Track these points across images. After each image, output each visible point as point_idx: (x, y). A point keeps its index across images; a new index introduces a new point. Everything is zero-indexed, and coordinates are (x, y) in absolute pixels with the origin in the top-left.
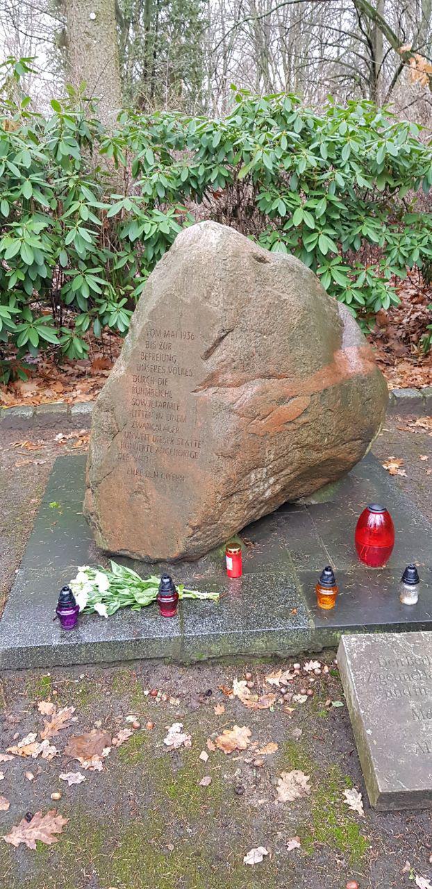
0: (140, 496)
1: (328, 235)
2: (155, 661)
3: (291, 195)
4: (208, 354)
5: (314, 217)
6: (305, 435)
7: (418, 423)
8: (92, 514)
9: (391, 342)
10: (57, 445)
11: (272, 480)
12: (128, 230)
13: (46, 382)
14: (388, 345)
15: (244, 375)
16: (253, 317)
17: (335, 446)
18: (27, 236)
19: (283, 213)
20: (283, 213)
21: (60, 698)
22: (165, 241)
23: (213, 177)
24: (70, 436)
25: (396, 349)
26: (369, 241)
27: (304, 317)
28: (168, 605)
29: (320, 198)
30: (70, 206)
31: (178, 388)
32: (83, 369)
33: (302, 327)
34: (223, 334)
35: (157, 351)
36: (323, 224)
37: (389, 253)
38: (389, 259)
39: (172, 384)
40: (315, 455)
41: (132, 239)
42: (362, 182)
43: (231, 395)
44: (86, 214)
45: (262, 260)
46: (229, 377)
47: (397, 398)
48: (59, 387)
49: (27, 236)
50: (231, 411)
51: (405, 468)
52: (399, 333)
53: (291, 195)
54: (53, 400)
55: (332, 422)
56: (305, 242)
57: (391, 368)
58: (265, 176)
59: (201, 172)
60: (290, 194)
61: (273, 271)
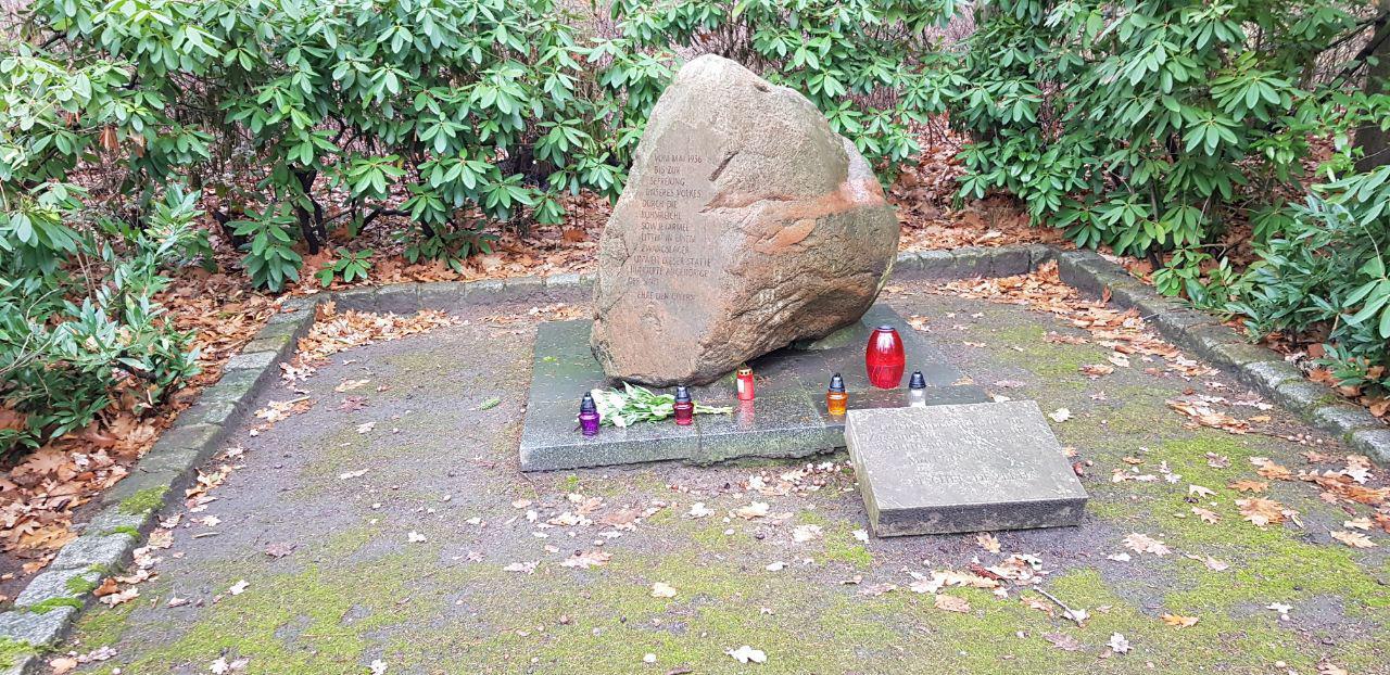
0: (650, 319)
1: (834, 77)
2: (673, 463)
3: (792, 34)
4: (715, 176)
5: (818, 57)
6: (812, 258)
7: (949, 286)
8: (601, 344)
9: (920, 204)
10: (533, 317)
11: (780, 304)
12: (610, 76)
13: (511, 255)
14: (916, 207)
15: (750, 195)
16: (756, 142)
17: (844, 275)
18: (503, 84)
19: (782, 52)
20: (782, 52)
21: (586, 490)
22: (652, 88)
23: (704, 16)
24: (547, 309)
25: (926, 212)
26: (882, 83)
27: (805, 142)
28: (682, 415)
29: (824, 36)
30: (546, 52)
31: (687, 210)
32: (552, 242)
33: (806, 152)
35: (666, 175)
36: (828, 64)
37: (906, 96)
38: (906, 102)
39: (681, 205)
40: (823, 283)
41: (615, 86)
42: (869, 18)
43: (737, 214)
44: (564, 60)
45: (762, 89)
46: (736, 197)
47: (923, 260)
48: (527, 261)
49: (503, 84)
51: (929, 324)
52: (929, 195)
53: (792, 34)
54: (520, 273)
55: (839, 250)
56: (810, 84)
57: (918, 231)
58: (761, 14)
59: (691, 10)
60: (790, 32)
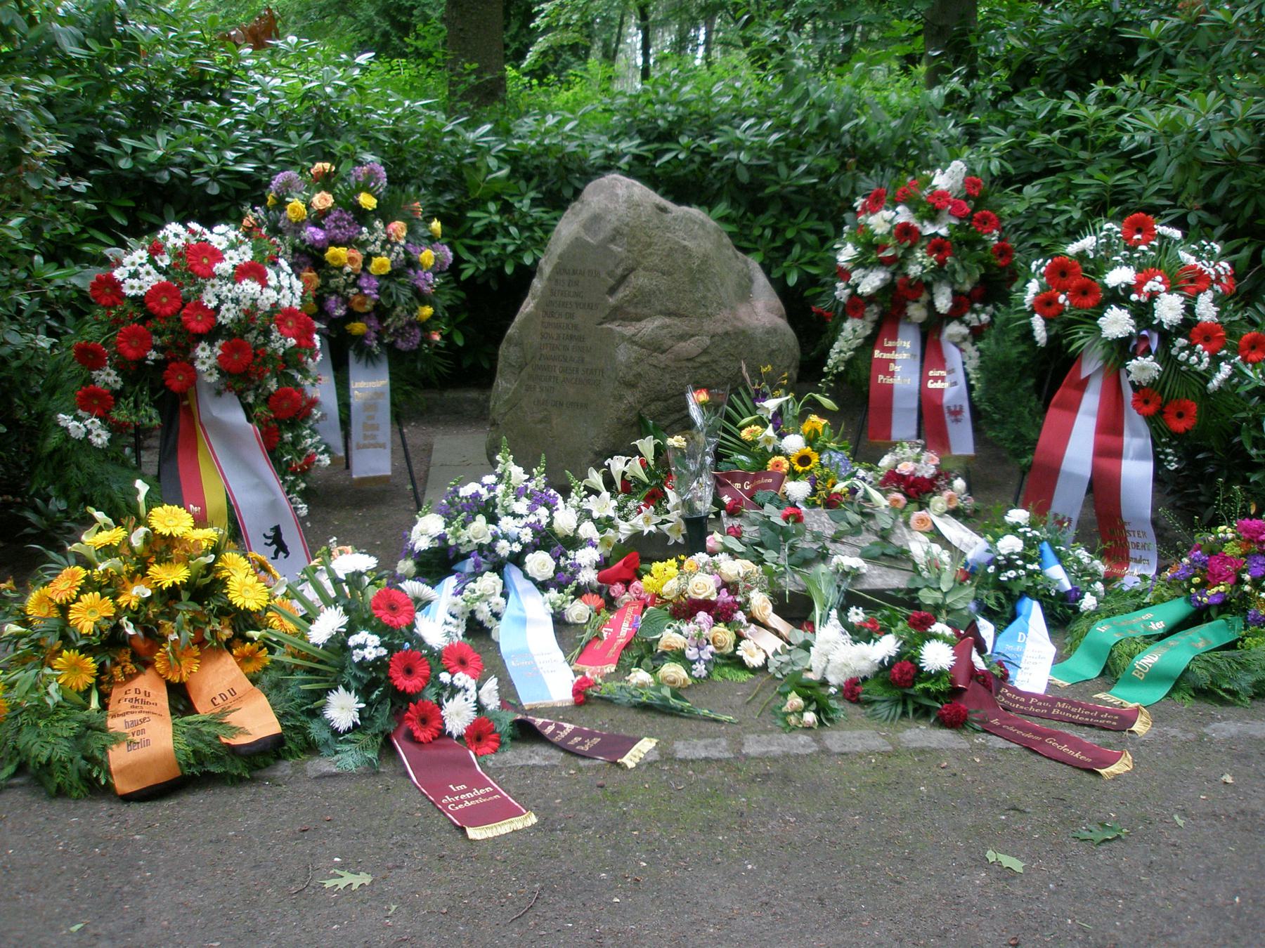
4: (612, 291)
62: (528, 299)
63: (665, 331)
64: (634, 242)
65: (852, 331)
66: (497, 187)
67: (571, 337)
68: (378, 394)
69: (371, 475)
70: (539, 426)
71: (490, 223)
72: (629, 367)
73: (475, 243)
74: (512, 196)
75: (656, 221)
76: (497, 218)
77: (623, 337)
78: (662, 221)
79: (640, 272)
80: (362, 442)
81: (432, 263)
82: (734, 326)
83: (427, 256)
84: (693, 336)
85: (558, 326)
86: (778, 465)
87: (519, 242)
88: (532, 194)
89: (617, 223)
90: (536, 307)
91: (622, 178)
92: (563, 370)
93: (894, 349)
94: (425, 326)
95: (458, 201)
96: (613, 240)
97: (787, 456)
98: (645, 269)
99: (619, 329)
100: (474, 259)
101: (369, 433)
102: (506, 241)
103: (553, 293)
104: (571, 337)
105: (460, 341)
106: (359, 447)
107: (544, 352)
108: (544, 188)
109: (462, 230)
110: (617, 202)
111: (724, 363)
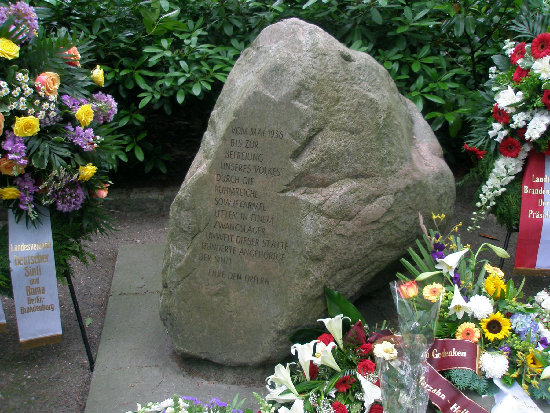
4: (297, 154)
24: (87, 310)
34: (313, 133)
50: (320, 212)
61: (359, 69)
62: (199, 156)
63: (353, 196)
64: (321, 97)
65: (504, 168)
66: (169, 26)
67: (250, 205)
68: (39, 257)
69: (40, 336)
70: (215, 299)
71: (164, 57)
72: (316, 240)
73: (151, 74)
74: (181, 33)
75: (343, 72)
76: (169, 54)
77: (309, 207)
78: (347, 71)
79: (328, 132)
80: (26, 306)
81: (90, 119)
82: (413, 179)
83: (85, 112)
84: (379, 196)
85: (235, 192)
86: (468, 333)
87: (188, 75)
88: (199, 32)
89: (302, 77)
90: (210, 168)
91: (302, 22)
92: (241, 241)
93: (542, 185)
94: (90, 186)
95: (137, 37)
96: (297, 95)
97: (476, 321)
98: (333, 128)
99: (304, 197)
100: (150, 89)
101: (33, 297)
102: (177, 74)
103: (228, 155)
104: (250, 205)
105: (140, 156)
106: (23, 311)
107: (219, 220)
108: (208, 26)
109: (139, 63)
110: (300, 51)
111: (404, 218)
